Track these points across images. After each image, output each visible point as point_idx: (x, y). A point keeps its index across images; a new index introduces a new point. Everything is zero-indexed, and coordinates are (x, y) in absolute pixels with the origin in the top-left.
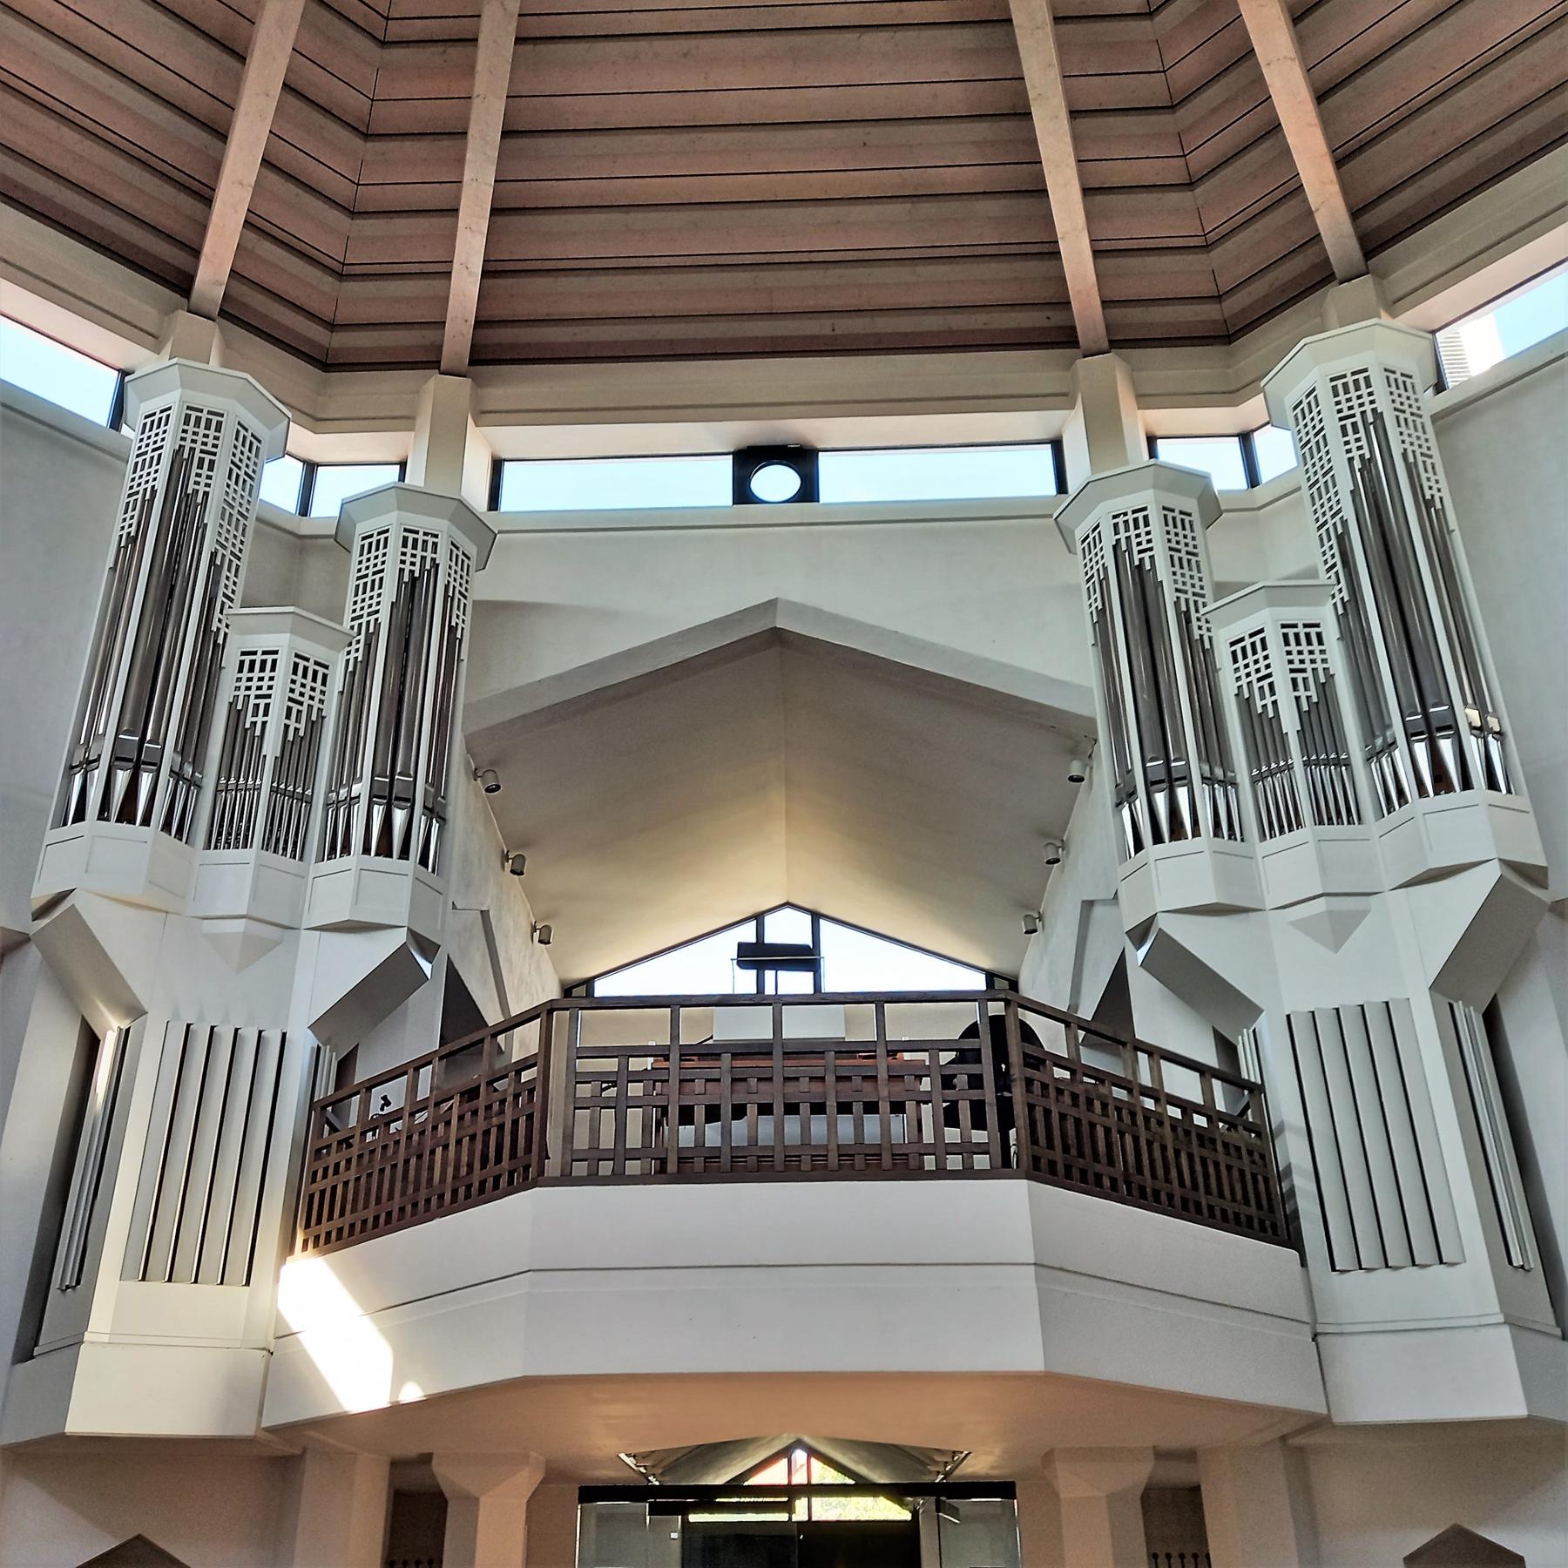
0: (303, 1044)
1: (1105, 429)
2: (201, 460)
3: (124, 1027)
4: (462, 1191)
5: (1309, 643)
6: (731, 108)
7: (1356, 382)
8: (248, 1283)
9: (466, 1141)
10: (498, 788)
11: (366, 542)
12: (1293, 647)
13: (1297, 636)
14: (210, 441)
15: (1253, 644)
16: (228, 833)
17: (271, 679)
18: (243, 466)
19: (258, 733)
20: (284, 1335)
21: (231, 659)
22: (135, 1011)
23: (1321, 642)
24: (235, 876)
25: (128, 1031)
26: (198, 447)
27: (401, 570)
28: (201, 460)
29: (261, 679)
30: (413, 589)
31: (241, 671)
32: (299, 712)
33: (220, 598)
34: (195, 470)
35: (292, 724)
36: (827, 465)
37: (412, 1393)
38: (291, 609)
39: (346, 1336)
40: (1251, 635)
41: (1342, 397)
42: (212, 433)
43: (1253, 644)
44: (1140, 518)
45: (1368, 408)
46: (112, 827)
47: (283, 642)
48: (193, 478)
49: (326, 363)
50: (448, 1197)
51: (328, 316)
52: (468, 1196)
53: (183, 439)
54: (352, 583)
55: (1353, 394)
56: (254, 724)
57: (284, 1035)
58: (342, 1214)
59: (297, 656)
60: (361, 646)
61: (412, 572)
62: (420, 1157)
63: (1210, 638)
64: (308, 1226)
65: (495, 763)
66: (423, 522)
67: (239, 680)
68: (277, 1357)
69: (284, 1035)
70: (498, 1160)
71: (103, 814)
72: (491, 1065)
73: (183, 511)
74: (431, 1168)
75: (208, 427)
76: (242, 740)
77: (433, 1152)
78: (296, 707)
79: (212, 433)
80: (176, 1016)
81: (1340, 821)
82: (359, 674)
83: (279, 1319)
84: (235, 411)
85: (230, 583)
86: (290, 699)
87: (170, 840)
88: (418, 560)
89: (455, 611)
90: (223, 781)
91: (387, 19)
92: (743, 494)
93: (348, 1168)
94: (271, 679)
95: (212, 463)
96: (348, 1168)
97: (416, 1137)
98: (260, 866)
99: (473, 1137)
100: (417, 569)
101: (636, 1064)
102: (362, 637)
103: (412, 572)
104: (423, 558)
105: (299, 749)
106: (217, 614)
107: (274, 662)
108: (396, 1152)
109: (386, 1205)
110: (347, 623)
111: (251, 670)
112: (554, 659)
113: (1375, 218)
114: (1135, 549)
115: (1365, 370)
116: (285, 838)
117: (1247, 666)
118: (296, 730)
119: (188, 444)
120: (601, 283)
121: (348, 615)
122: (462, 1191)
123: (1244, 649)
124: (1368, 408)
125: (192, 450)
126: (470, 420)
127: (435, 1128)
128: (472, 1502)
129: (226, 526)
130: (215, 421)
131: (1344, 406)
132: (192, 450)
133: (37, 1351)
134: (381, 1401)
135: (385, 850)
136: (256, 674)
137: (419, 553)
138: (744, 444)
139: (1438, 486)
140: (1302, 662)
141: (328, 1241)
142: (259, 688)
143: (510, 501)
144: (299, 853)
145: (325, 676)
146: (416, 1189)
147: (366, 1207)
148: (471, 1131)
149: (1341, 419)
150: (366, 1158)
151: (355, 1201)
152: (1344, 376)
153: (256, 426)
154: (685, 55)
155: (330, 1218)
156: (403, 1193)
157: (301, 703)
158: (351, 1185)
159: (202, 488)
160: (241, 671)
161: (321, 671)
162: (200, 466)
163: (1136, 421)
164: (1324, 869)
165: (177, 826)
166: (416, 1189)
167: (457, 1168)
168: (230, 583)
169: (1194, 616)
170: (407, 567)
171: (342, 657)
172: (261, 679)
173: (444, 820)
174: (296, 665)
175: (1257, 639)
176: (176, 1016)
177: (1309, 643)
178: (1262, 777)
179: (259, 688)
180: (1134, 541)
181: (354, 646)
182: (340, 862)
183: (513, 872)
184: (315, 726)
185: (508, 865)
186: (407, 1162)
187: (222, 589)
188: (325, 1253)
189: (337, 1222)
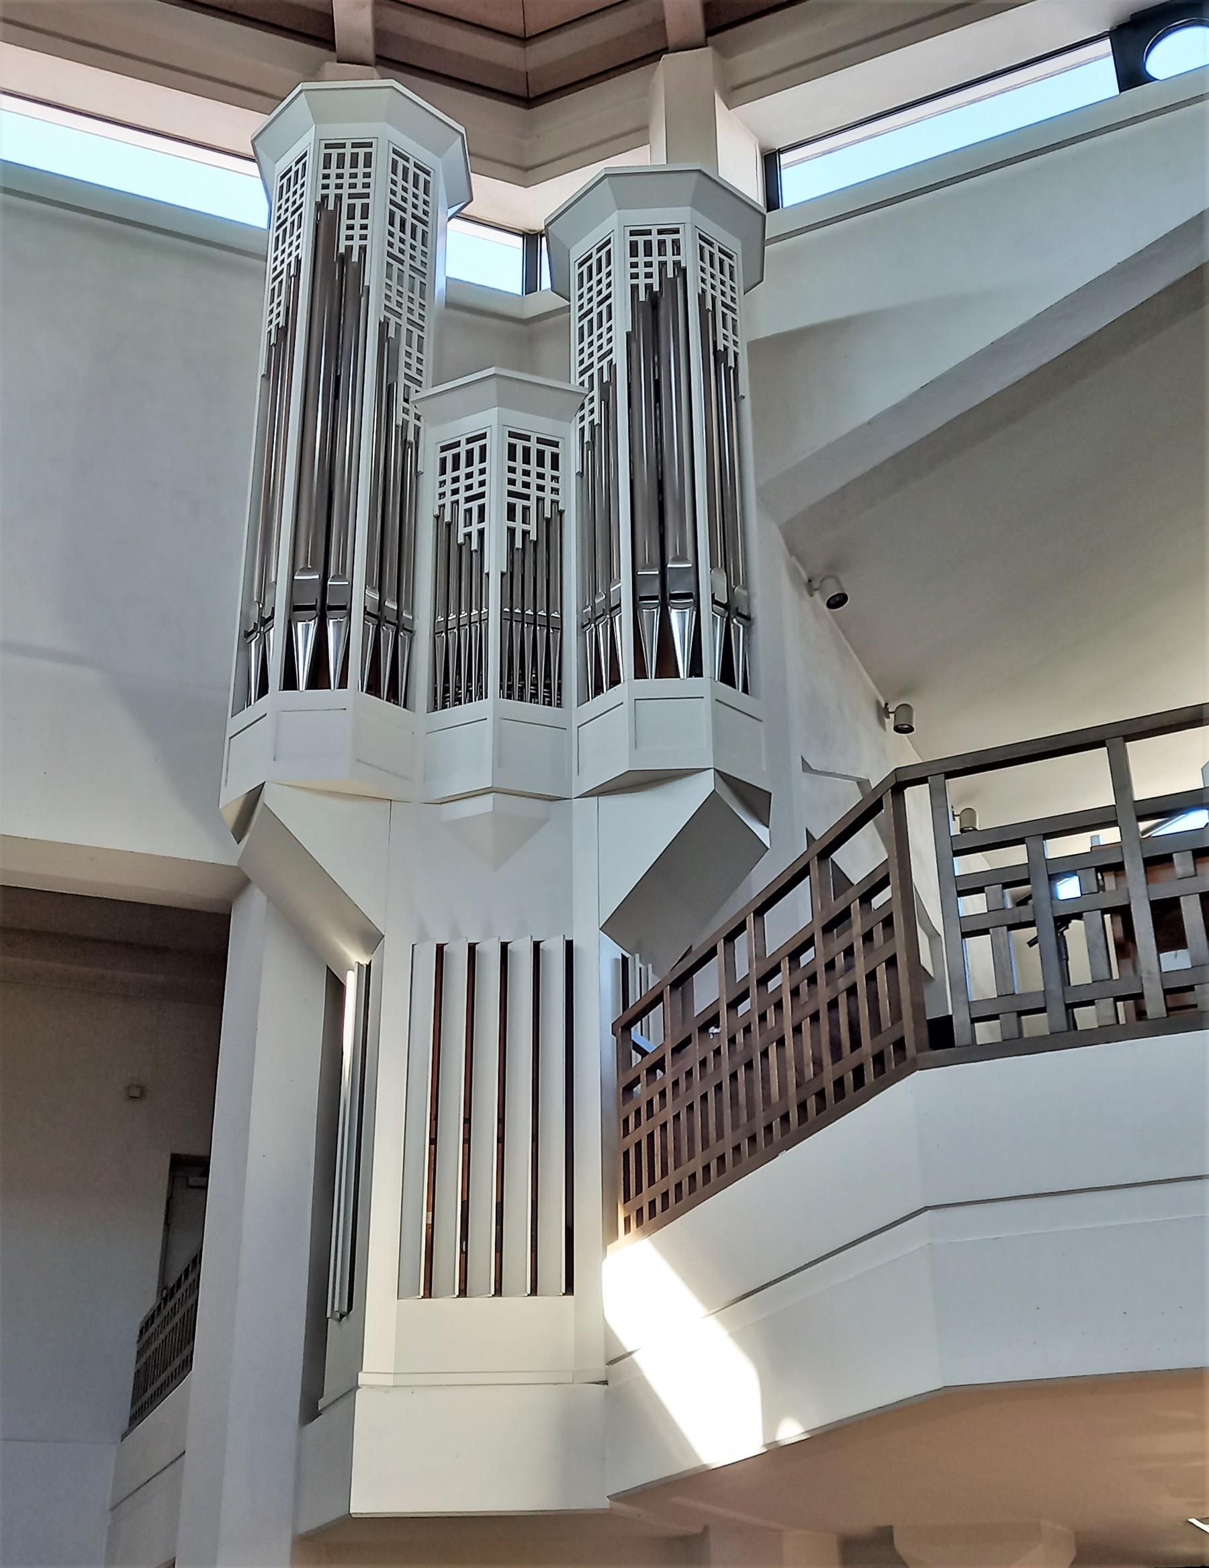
0: (600, 959)
2: (352, 208)
3: (365, 962)
4: (812, 1103)
5: (541, 463)
7: (355, 157)
8: (570, 1289)
9: (806, 1025)
10: (911, 729)
11: (585, 268)
12: (519, 465)
13: (526, 451)
14: (360, 180)
16: (457, 684)
17: (482, 472)
18: (408, 206)
19: (474, 546)
20: (618, 1358)
22: (371, 939)
23: (555, 466)
25: (369, 967)
26: (345, 192)
27: (635, 288)
28: (352, 208)
30: (654, 312)
31: (443, 472)
32: (526, 509)
33: (402, 381)
34: (345, 221)
35: (519, 525)
37: (791, 1431)
38: (491, 371)
39: (691, 1353)
40: (469, 441)
42: (361, 170)
45: (548, 496)
46: (302, 694)
47: (490, 421)
48: (344, 232)
49: (528, 97)
50: (794, 1116)
51: (516, 27)
52: (821, 1108)
53: (325, 187)
54: (575, 326)
56: (469, 535)
57: (569, 945)
58: (664, 1172)
59: (511, 435)
60: (596, 404)
62: (749, 1066)
64: (627, 1198)
65: (834, 568)
66: (653, 217)
67: (443, 483)
68: (611, 1392)
69: (569, 945)
70: (856, 1043)
71: (290, 682)
73: (337, 275)
74: (766, 1079)
75: (354, 164)
76: (460, 561)
77: (765, 1054)
78: (520, 504)
79: (361, 170)
80: (423, 935)
82: (597, 442)
83: (609, 1337)
84: (386, 135)
85: (413, 362)
86: (511, 494)
87: (381, 705)
88: (655, 270)
89: (720, 330)
90: (440, 619)
92: (1131, 75)
93: (663, 1105)
94: (482, 472)
95: (365, 208)
96: (663, 1105)
97: (740, 1038)
98: (501, 719)
99: (815, 1017)
100: (655, 281)
101: (1057, 848)
102: (596, 393)
104: (663, 265)
105: (534, 558)
107: (483, 449)
108: (717, 1066)
109: (717, 1148)
110: (575, 380)
112: (881, 388)
116: (532, 677)
118: (525, 533)
119: (332, 192)
121: (576, 369)
122: (812, 1103)
125: (339, 198)
126: (719, 104)
127: (763, 1018)
129: (395, 287)
130: (360, 154)
132: (339, 198)
133: (322, 1403)
134: (755, 1447)
135: (667, 668)
136: (463, 470)
137: (655, 259)
141: (652, 1214)
142: (469, 488)
143: (791, 195)
144: (551, 694)
145: (555, 457)
146: (751, 1116)
147: (691, 1156)
148: (810, 1010)
150: (683, 1084)
151: (677, 1149)
152: (649, 233)
153: (418, 152)
155: (652, 1181)
156: (735, 1126)
157: (527, 497)
158: (670, 1127)
159: (356, 243)
160: (443, 472)
161: (548, 450)
162: (351, 216)
165: (386, 682)
166: (751, 1116)
167: (800, 1071)
168: (413, 362)
170: (642, 282)
171: (575, 426)
173: (748, 618)
174: (512, 448)
175: (476, 446)
176: (423, 935)
177: (541, 463)
179: (469, 488)
181: (588, 408)
182: (610, 696)
183: (897, 729)
184: (551, 525)
185: (890, 722)
186: (734, 1076)
187: (402, 370)
188: (648, 1232)
189: (661, 1185)
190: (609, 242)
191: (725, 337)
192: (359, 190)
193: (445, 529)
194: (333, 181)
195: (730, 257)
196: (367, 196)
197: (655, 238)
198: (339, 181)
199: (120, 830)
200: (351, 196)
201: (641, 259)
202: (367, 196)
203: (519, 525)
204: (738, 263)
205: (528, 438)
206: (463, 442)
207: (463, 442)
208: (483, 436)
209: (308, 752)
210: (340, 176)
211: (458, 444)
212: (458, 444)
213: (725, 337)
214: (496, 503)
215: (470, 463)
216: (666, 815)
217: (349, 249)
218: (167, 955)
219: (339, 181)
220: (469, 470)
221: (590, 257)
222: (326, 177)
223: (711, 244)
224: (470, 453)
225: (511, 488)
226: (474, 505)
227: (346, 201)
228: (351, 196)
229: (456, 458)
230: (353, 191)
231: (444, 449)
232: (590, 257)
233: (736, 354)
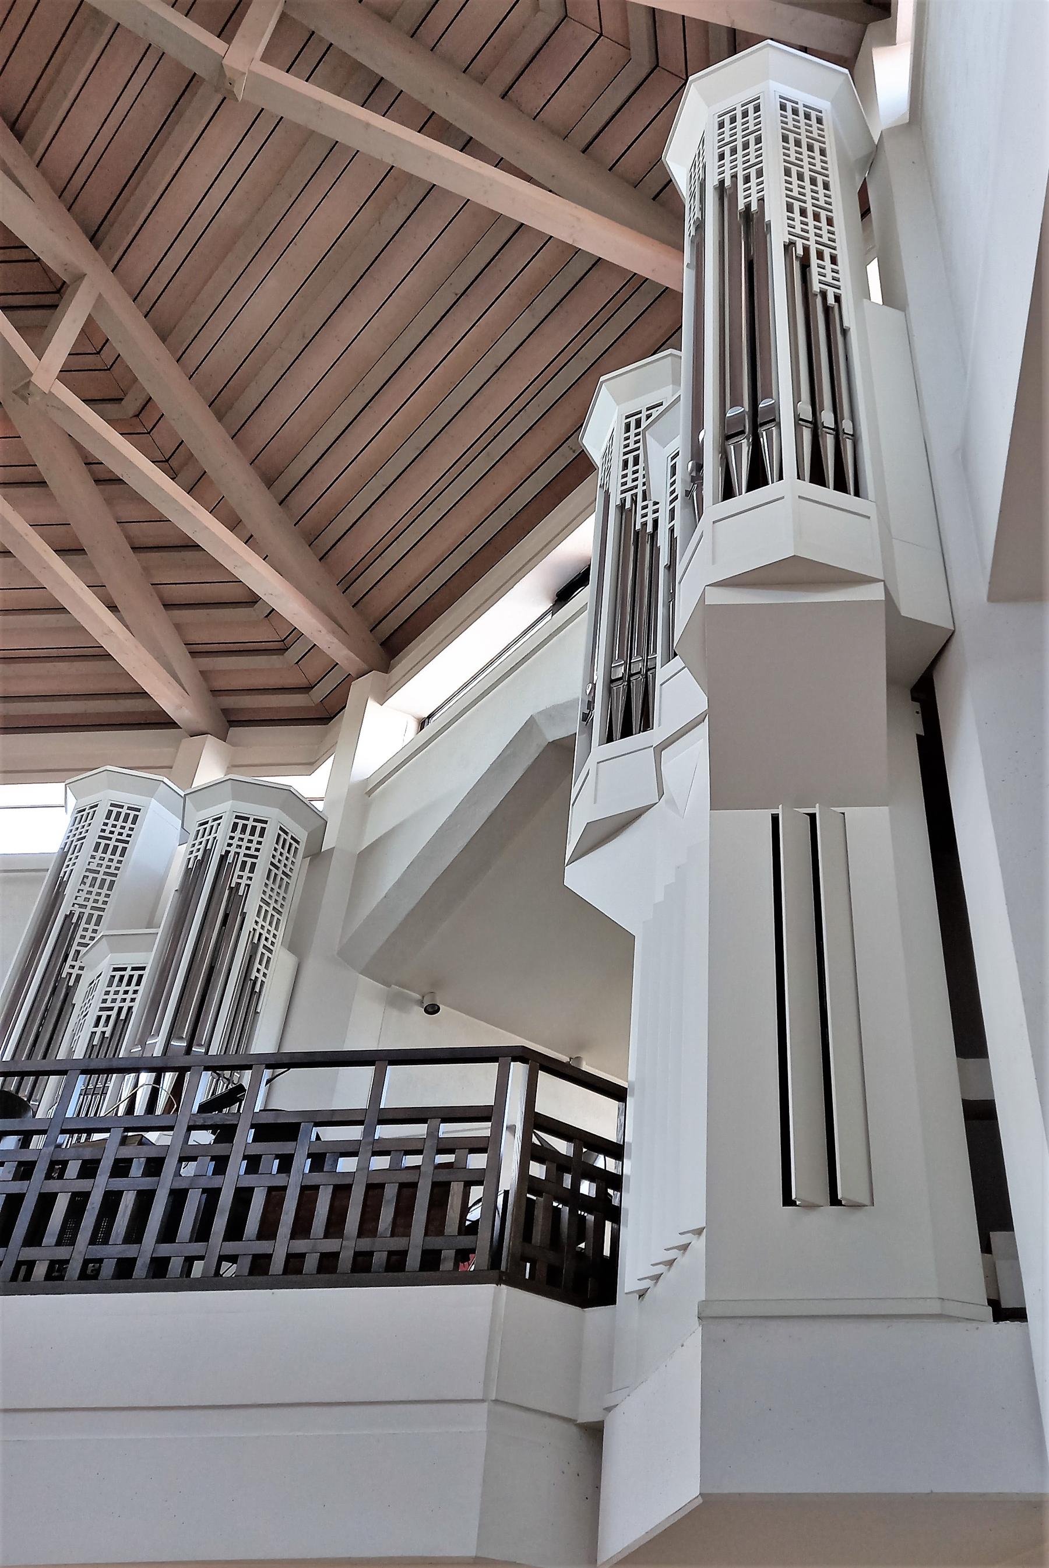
2: (244, 863)
7: (254, 828)
15: (131, 977)
26: (243, 851)
28: (244, 863)
29: (114, 826)
34: (237, 872)
40: (133, 969)
41: (111, 822)
43: (131, 977)
44: (259, 827)
53: (230, 845)
55: (120, 823)
59: (281, 828)
63: (263, 982)
66: (253, 810)
72: (177, 1174)
75: (252, 834)
91: (167, 461)
111: (117, 819)
115: (266, 822)
119: (233, 849)
131: (109, 828)
149: (100, 837)
152: (248, 819)
162: (243, 869)
172: (123, 828)
175: (136, 973)
179: (120, 834)
190: (221, 818)
192: (252, 852)
194: (235, 842)
195: (297, 842)
196: (256, 857)
197: (250, 824)
198: (249, 845)
200: (246, 855)
201: (237, 834)
204: (301, 848)
206: (129, 969)
207: (129, 969)
210: (242, 839)
211: (125, 969)
212: (125, 969)
215: (129, 984)
219: (249, 845)
220: (127, 988)
221: (207, 823)
222: (232, 838)
223: (286, 833)
224: (131, 977)
227: (241, 858)
228: (246, 855)
229: (122, 977)
230: (248, 852)
231: (115, 970)
232: (207, 823)
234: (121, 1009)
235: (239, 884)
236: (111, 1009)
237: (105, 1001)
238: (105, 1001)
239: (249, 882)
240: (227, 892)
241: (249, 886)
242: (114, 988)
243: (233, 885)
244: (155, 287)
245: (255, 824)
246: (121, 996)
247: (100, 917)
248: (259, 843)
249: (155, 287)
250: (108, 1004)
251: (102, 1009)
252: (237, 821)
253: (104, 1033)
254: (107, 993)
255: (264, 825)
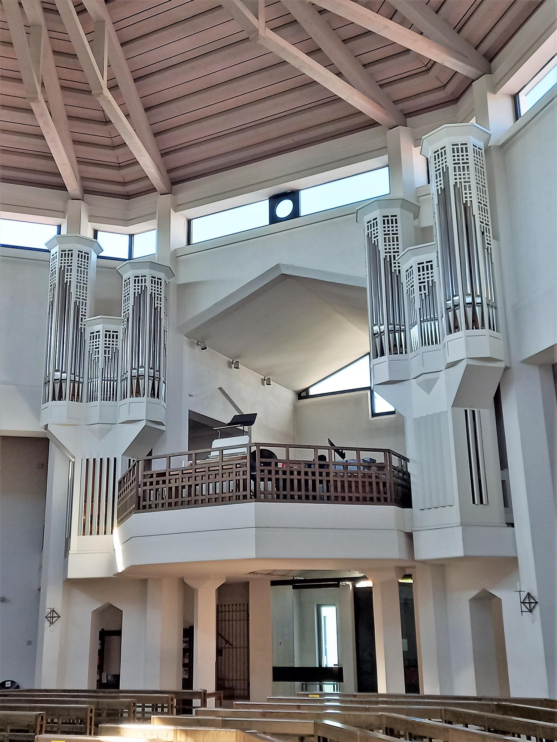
1: (75, 225)
2: (68, 269)
6: (221, 77)
10: (206, 348)
21: (87, 336)
23: (117, 338)
24: (95, 409)
27: (135, 292)
36: (304, 196)
40: (441, 149)
43: (442, 152)
47: (99, 327)
49: (128, 196)
61: (138, 292)
71: (54, 399)
81: (429, 345)
88: (140, 287)
89: (156, 302)
98: (101, 406)
100: (140, 291)
103: (138, 292)
104: (142, 286)
106: (80, 323)
112: (206, 302)
113: (485, 47)
114: (373, 236)
117: (424, 274)
120: (203, 147)
123: (423, 267)
124: (430, 279)
128: (197, 590)
137: (140, 284)
138: (271, 195)
139: (474, 198)
140: (109, 344)
149: (420, 283)
154: (194, 67)
157: (109, 348)
162: (465, 189)
163: (87, 231)
164: (467, 349)
169: (393, 261)
170: (136, 291)
175: (443, 150)
178: (424, 321)
180: (373, 233)
185: (233, 366)
187: (81, 313)
191: (157, 303)
193: (90, 355)
199: (22, 425)
202: (71, 266)
203: (107, 355)
205: (110, 331)
208: (445, 147)
209: (56, 418)
211: (93, 333)
213: (157, 303)
214: (101, 350)
216: (137, 429)
217: (67, 281)
218: (38, 447)
225: (454, 162)
226: (97, 350)
233: (160, 307)
234: (443, 167)
235: (466, 201)
236: (439, 169)
237: (436, 167)
238: (436, 167)
239: (471, 199)
240: (462, 206)
241: (471, 201)
242: (437, 160)
243: (464, 202)
244: (125, 23)
245: (464, 165)
246: (441, 162)
247: (431, 265)
248: (467, 155)
249: (125, 23)
250: (438, 168)
251: (436, 171)
252: (455, 165)
253: (441, 188)
254: (436, 164)
255: (467, 165)
